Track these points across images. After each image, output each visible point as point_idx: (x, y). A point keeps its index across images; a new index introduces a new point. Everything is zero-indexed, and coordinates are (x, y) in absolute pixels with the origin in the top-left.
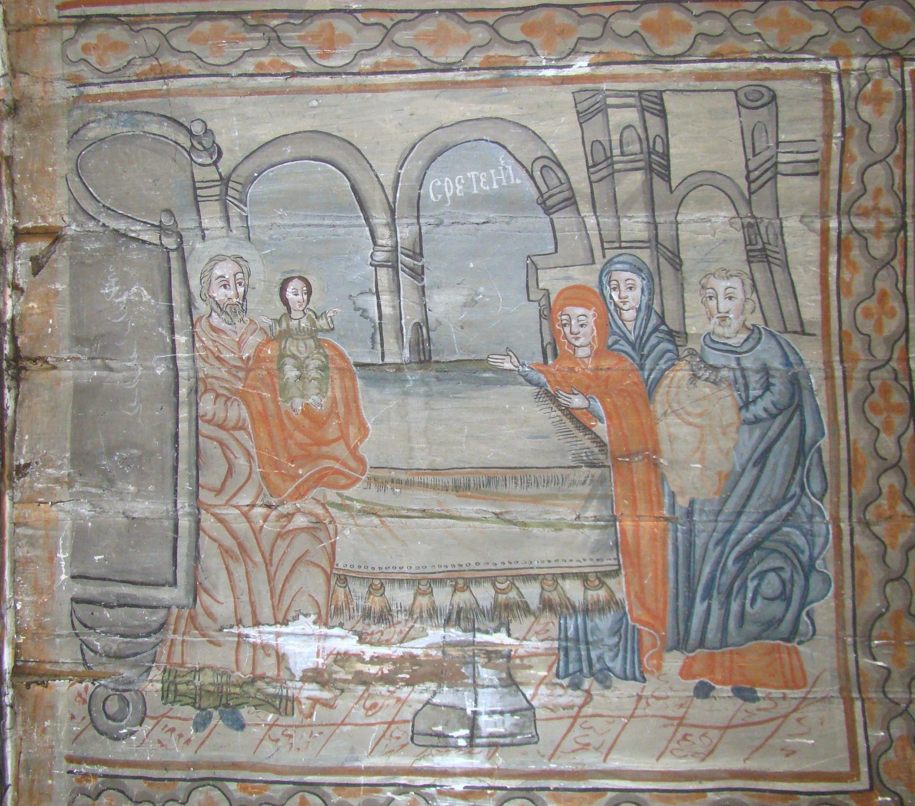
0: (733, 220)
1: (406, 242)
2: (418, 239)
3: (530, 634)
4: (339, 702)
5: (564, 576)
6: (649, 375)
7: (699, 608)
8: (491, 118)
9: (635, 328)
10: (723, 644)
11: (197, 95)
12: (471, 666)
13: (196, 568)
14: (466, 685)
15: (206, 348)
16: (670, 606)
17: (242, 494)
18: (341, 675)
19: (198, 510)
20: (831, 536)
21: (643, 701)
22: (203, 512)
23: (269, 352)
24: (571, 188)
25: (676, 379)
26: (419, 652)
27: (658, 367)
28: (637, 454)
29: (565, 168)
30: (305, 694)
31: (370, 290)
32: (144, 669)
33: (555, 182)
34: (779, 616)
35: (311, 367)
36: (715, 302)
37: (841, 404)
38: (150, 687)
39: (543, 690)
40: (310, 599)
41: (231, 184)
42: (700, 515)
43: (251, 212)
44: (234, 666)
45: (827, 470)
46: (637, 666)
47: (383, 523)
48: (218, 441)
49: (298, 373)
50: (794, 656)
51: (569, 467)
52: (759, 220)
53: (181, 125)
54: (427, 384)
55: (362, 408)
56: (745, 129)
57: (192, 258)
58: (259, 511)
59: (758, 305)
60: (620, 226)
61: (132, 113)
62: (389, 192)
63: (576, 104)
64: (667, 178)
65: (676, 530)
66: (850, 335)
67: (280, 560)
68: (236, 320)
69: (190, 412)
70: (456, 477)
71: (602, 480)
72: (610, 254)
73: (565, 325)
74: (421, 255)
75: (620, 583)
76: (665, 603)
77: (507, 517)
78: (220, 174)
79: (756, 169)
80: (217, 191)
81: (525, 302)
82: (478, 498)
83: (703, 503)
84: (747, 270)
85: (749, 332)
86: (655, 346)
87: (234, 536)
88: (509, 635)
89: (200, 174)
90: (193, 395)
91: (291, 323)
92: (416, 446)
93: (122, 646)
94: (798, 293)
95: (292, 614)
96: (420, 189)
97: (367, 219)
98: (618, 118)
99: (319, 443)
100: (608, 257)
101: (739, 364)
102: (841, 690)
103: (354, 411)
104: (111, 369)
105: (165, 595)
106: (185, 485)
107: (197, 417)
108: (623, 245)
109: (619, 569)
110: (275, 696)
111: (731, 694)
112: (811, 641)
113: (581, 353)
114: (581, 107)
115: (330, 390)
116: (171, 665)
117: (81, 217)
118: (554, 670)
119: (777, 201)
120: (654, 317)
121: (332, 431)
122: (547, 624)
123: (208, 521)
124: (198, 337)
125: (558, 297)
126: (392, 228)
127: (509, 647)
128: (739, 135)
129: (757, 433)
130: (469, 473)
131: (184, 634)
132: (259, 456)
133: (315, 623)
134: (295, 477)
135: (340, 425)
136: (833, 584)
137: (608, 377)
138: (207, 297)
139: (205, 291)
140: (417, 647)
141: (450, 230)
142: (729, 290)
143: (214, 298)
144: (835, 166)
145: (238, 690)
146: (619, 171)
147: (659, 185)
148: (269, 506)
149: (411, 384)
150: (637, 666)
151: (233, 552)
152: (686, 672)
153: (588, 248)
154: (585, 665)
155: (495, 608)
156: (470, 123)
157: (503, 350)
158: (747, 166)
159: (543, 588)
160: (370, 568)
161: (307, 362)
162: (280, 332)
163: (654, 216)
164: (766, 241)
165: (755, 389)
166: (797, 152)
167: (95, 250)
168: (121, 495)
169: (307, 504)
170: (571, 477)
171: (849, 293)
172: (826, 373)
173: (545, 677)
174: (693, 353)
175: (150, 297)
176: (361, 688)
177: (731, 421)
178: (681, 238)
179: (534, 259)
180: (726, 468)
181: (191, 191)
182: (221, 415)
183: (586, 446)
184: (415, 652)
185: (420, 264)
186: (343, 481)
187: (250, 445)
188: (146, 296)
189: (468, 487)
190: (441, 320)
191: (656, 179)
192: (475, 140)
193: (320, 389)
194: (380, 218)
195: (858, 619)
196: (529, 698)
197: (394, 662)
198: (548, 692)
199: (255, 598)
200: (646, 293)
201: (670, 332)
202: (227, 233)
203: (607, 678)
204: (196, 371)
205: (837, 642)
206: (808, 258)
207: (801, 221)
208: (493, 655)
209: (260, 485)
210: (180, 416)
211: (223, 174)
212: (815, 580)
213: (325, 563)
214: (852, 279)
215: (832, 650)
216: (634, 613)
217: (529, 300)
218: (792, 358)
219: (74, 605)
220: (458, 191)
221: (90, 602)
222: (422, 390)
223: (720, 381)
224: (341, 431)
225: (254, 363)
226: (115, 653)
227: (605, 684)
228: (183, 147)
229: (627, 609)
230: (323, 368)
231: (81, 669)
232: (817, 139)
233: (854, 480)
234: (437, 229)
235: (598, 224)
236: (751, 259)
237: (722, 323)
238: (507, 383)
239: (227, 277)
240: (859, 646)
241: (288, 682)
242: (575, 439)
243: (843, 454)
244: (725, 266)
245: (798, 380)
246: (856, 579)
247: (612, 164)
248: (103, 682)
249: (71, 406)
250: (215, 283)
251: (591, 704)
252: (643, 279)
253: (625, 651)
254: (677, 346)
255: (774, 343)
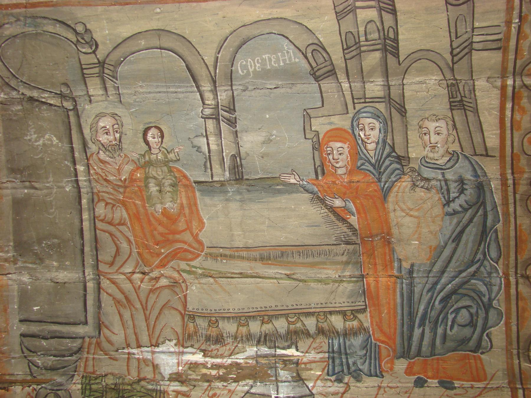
0: (441, 82)
1: (224, 102)
2: (232, 100)
3: (310, 350)
4: (193, 393)
5: (331, 313)
6: (385, 184)
7: (417, 332)
8: (277, 18)
9: (375, 155)
10: (432, 354)
11: (78, 5)
12: (274, 369)
13: (99, 313)
14: (271, 381)
15: (97, 174)
16: (398, 331)
17: (126, 265)
18: (194, 376)
19: (99, 276)
20: (503, 286)
21: (382, 390)
22: (102, 277)
23: (139, 175)
24: (332, 63)
25: (402, 187)
26: (242, 361)
27: (390, 180)
28: (377, 235)
29: (328, 50)
30: (172, 388)
31: (202, 134)
32: (70, 376)
33: (322, 60)
34: (468, 336)
35: (166, 184)
36: (428, 136)
37: (511, 200)
38: (74, 387)
39: (319, 383)
40: (172, 330)
41: (106, 66)
42: (418, 273)
43: (121, 84)
44: (127, 373)
45: (501, 244)
46: (378, 368)
47: (216, 281)
48: (109, 233)
49: (157, 188)
50: (479, 362)
51: (333, 245)
52: (458, 81)
53: (69, 26)
54: (240, 193)
55: (200, 210)
56: (450, 19)
57: (83, 115)
58: (137, 276)
59: (457, 138)
60: (365, 88)
61: (34, 17)
62: (211, 69)
63: (335, 7)
64: (396, 55)
65: (402, 283)
66: (519, 156)
67: (152, 307)
68: (115, 156)
69: (90, 215)
70: (261, 252)
71: (354, 252)
72: (358, 107)
73: (329, 154)
74: (234, 110)
75: (366, 317)
76: (395, 329)
77: (295, 277)
78: (98, 59)
79: (457, 48)
80: (96, 70)
81: (303, 140)
82: (276, 265)
83: (420, 265)
84: (450, 115)
85: (451, 156)
86: (388, 167)
87: (123, 293)
88: (297, 350)
89: (84, 59)
90: (91, 203)
91: (152, 156)
92: (235, 233)
93: (54, 363)
94: (484, 129)
95: (161, 340)
96: (232, 67)
97: (198, 87)
98: (363, 16)
99: (174, 232)
100: (357, 108)
101: (443, 176)
102: (509, 383)
103: (195, 212)
104: (36, 189)
105: (80, 330)
106: (89, 261)
107: (94, 217)
108: (367, 100)
109: (366, 308)
110: (153, 390)
111: (438, 385)
112: (490, 352)
113: (340, 171)
114: (338, 9)
115: (179, 198)
116: (87, 373)
117: (8, 90)
118: (326, 371)
119: (472, 68)
120: (387, 147)
121: (182, 225)
122: (321, 342)
123: (105, 283)
124: (92, 166)
125: (324, 136)
126: (215, 93)
127: (298, 357)
128: (446, 25)
129: (455, 221)
130: (270, 249)
131: (94, 354)
132: (136, 241)
133: (176, 345)
134: (159, 254)
135: (186, 221)
136: (504, 316)
137: (358, 187)
138: (96, 141)
139: (94, 137)
140: (240, 358)
141: (253, 93)
142: (437, 129)
143: (100, 141)
144: (513, 43)
145: (129, 387)
146: (365, 51)
147: (391, 60)
148: (144, 273)
149: (230, 194)
150: (378, 368)
151: (123, 302)
152: (409, 372)
153: (344, 103)
154: (345, 368)
155: (288, 333)
156: (264, 22)
157: (289, 171)
158: (451, 45)
159: (318, 321)
160: (209, 310)
161: (163, 181)
162: (145, 162)
163: (388, 81)
164: (463, 95)
165: (454, 193)
166: (487, 35)
167: (19, 111)
168: (49, 268)
169: (167, 271)
170: (335, 251)
171: (519, 128)
172: (502, 180)
173: (320, 375)
174: (413, 170)
175: (58, 141)
176: (206, 384)
177: (437, 214)
178: (405, 95)
179: (308, 111)
180: (434, 244)
181: (80, 71)
182: (110, 216)
183: (343, 231)
184: (238, 361)
185: (234, 116)
186: (190, 256)
187: (129, 235)
188: (55, 141)
189: (269, 258)
190: (248, 152)
191: (389, 56)
192: (268, 33)
193: (173, 198)
194: (206, 87)
195: (520, 338)
196: (310, 388)
197: (225, 367)
198: (322, 384)
199: (138, 330)
200: (382, 132)
201: (398, 157)
202: (106, 98)
203: (359, 375)
204: (92, 188)
205: (507, 353)
206: (491, 106)
207: (487, 81)
208: (288, 363)
209: (137, 259)
210: (84, 217)
211: (100, 59)
212: (492, 313)
213: (180, 308)
214: (521, 119)
215: (503, 358)
216: (376, 335)
217: (306, 138)
218: (479, 172)
219: (22, 338)
220: (257, 68)
221: (33, 336)
222: (238, 197)
223: (431, 187)
224: (188, 225)
225: (129, 182)
226: (50, 366)
227: (358, 379)
228: (71, 41)
229: (371, 333)
230: (173, 185)
231: (29, 378)
232: (501, 24)
233: (519, 250)
234: (244, 93)
235: (350, 87)
236: (452, 107)
237: (433, 151)
238: (292, 192)
239: (108, 127)
240: (521, 355)
241: (160, 382)
242: (337, 227)
243: (512, 234)
244: (435, 113)
245: (483, 187)
246: (519, 313)
247: (360, 46)
248: (43, 385)
249: (11, 212)
250: (100, 131)
251: (349, 392)
252: (381, 123)
253: (371, 359)
254: (403, 166)
255: (467, 162)
